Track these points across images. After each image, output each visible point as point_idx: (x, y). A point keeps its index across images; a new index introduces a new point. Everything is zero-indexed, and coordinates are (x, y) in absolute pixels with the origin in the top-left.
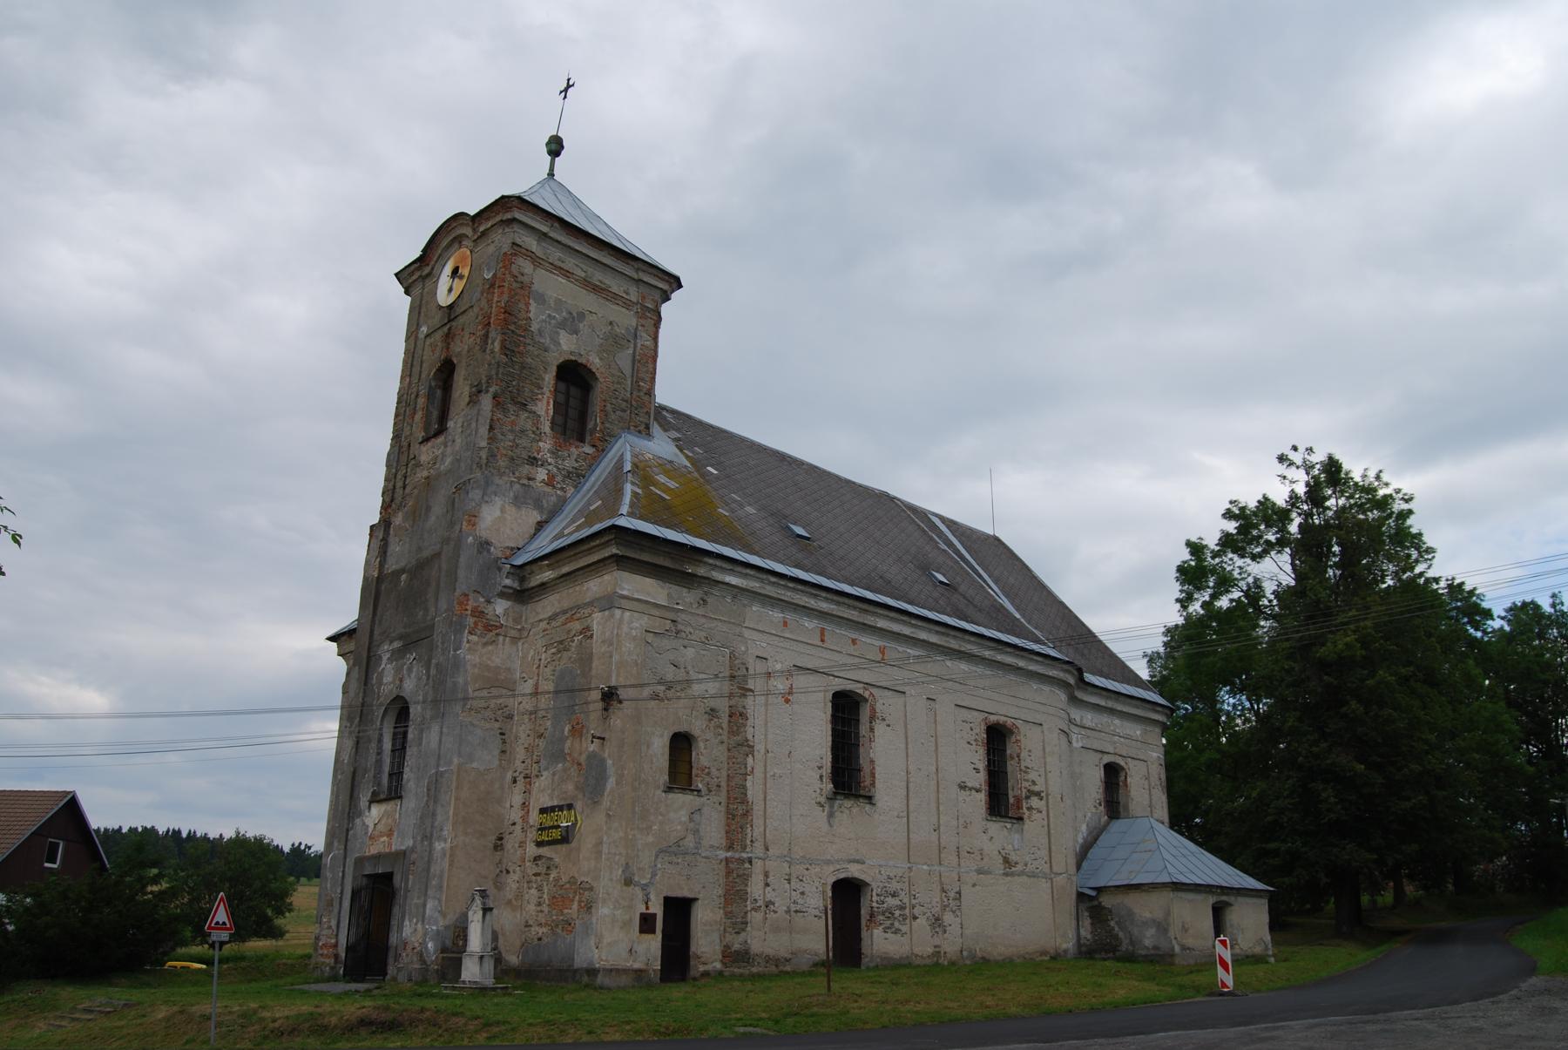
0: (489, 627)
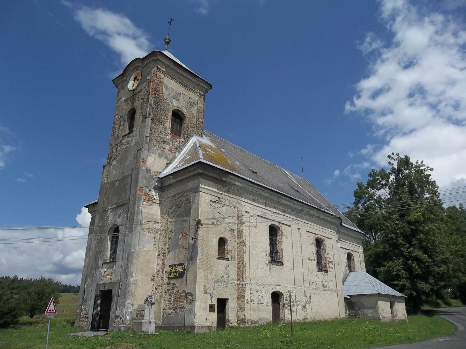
0: (150, 200)
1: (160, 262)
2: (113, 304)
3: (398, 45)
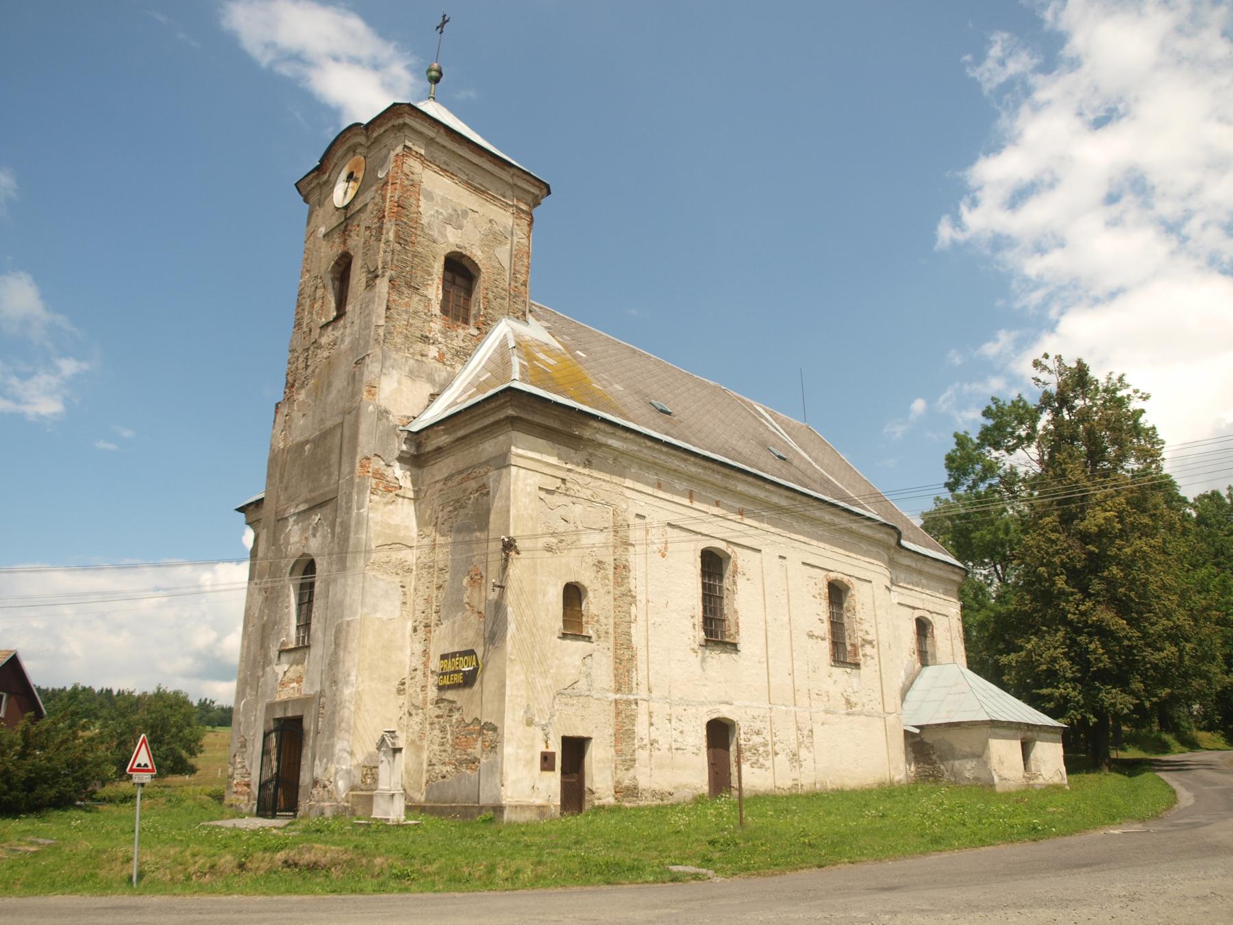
0: (388, 490)
1: (419, 648)
2: (307, 752)
3: (1075, 64)
